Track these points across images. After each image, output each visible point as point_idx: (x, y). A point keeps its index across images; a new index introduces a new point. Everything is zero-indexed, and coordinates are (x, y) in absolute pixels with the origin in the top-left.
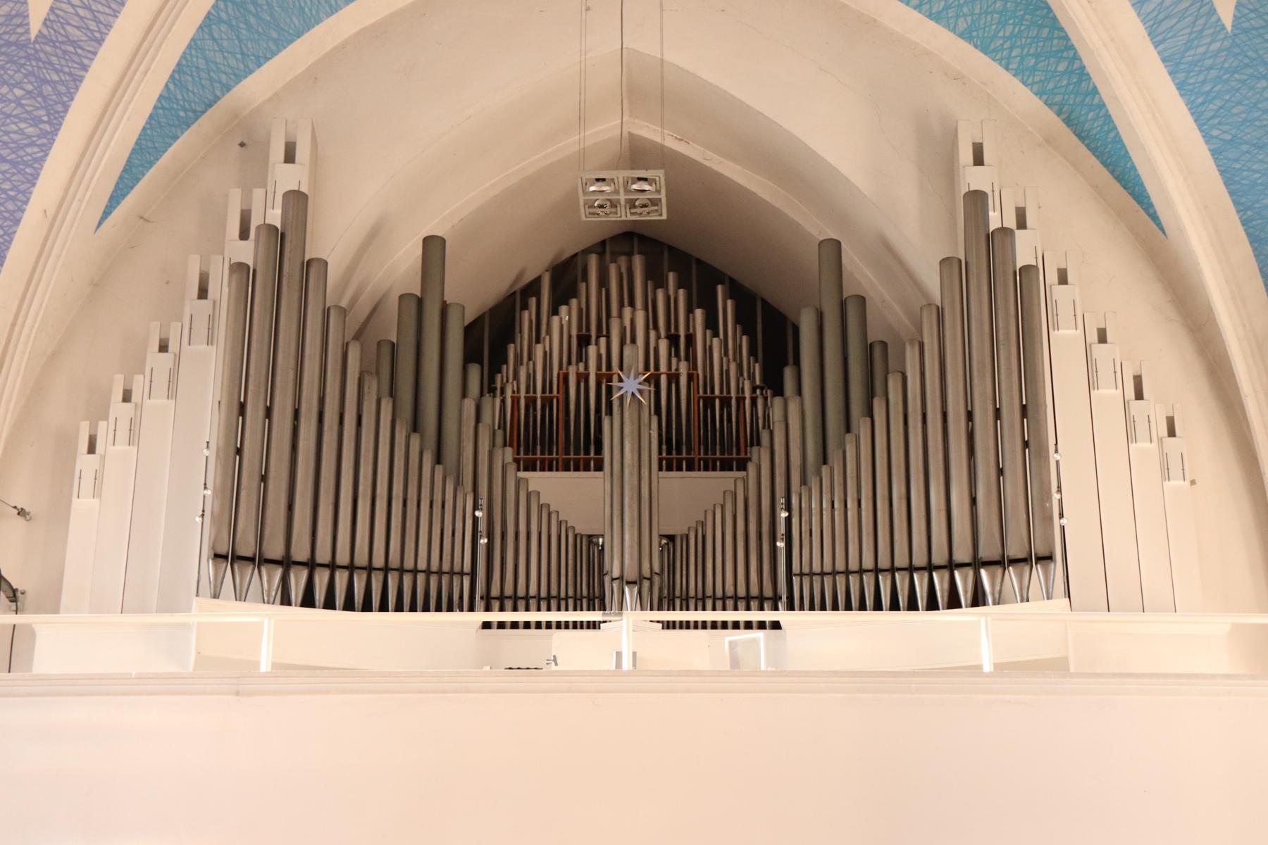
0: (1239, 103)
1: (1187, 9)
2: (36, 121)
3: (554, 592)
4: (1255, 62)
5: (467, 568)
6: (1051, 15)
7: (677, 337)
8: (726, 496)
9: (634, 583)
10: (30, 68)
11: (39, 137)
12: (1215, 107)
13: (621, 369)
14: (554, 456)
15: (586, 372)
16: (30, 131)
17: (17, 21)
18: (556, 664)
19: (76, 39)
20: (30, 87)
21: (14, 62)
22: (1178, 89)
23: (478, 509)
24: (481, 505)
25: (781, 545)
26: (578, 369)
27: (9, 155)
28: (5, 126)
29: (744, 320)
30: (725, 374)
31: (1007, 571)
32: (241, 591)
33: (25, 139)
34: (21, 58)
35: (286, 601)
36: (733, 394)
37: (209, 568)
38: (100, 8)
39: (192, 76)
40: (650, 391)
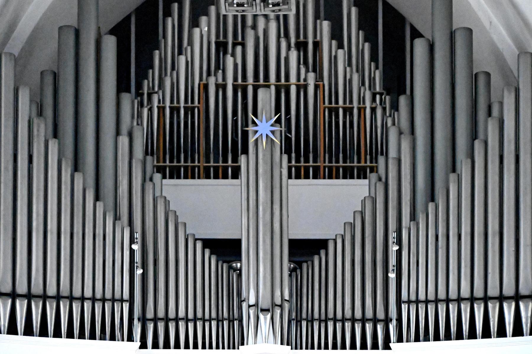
3: (199, 315)
5: (126, 296)
8: (346, 227)
9: (268, 310)
14: (196, 163)
23: (134, 243)
24: (137, 238)
25: (392, 276)
26: (217, 80)
30: (348, 83)
36: (355, 104)
40: (281, 131)
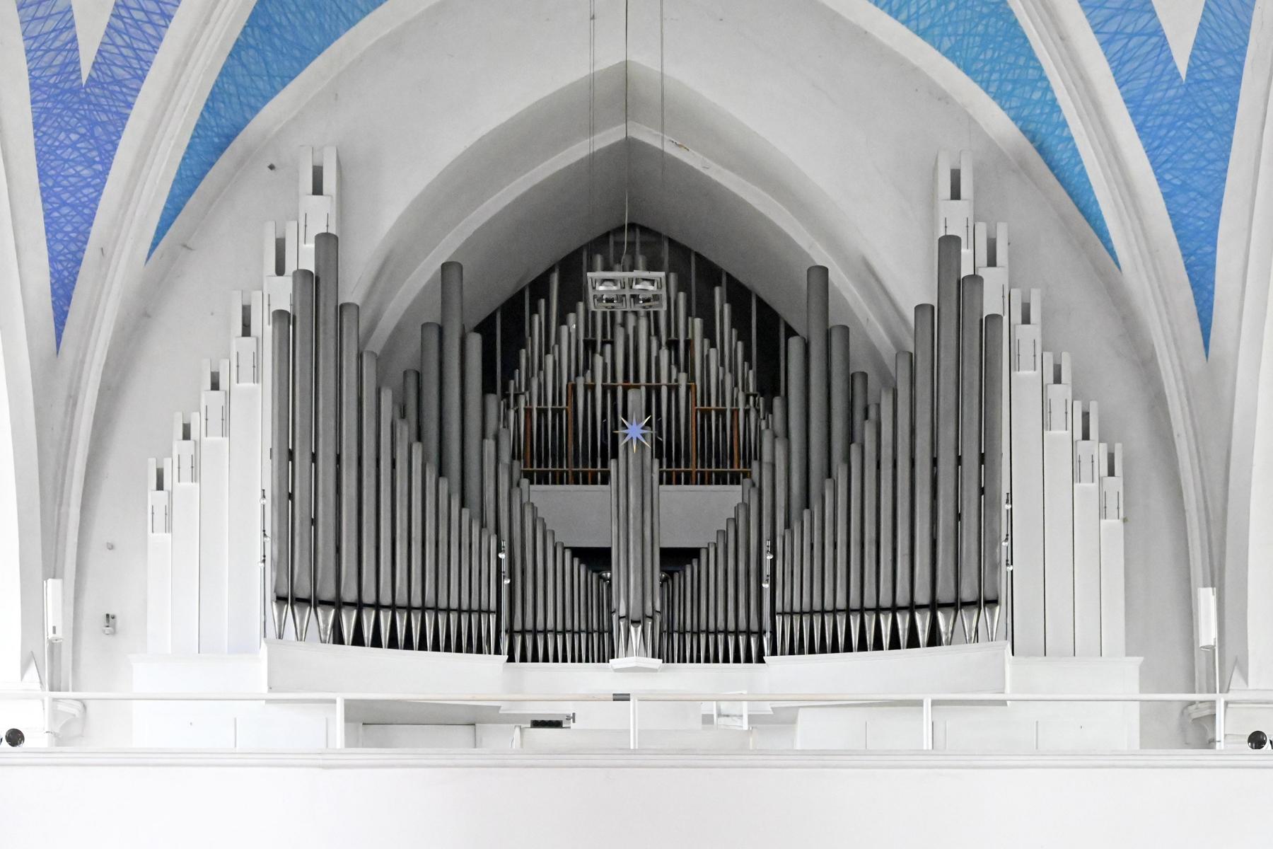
0: (1190, 151)
1: (1148, 53)
2: (90, 163)
4: (1205, 113)
5: (493, 606)
6: (1027, 45)
7: (676, 343)
9: (639, 622)
10: (82, 112)
11: (93, 177)
12: (1169, 152)
13: (625, 416)
15: (593, 383)
16: (86, 173)
17: (70, 69)
18: (574, 721)
19: (120, 78)
20: (83, 131)
21: (69, 108)
22: (1137, 130)
25: (766, 586)
27: (69, 198)
28: (65, 170)
29: (740, 321)
30: (721, 384)
31: (959, 612)
32: (302, 631)
33: (81, 181)
34: (75, 103)
35: (339, 639)
36: (728, 406)
37: (273, 609)
38: (141, 46)
39: (223, 102)
40: (652, 434)
